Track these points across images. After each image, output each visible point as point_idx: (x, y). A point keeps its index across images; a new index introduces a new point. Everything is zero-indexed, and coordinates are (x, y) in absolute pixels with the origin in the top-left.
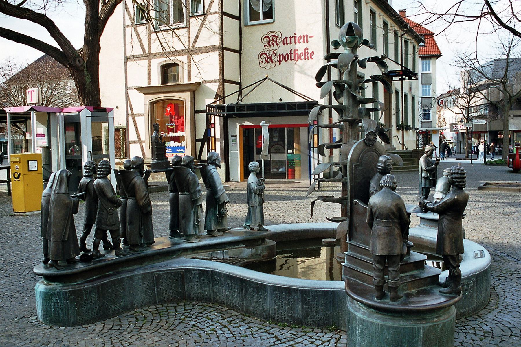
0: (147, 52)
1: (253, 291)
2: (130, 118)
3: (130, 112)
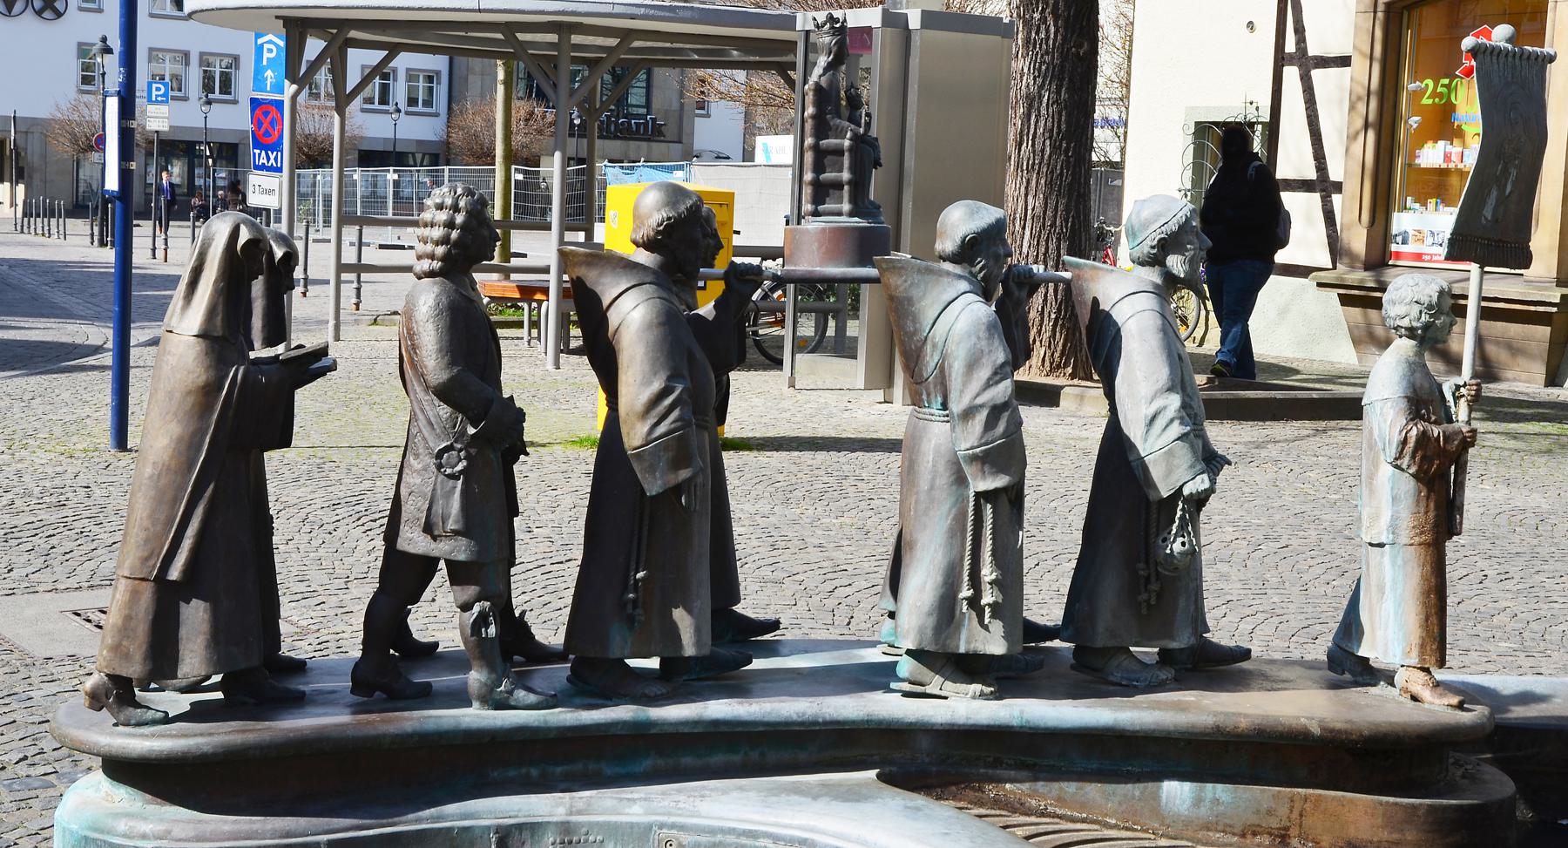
3: (1290, 47)
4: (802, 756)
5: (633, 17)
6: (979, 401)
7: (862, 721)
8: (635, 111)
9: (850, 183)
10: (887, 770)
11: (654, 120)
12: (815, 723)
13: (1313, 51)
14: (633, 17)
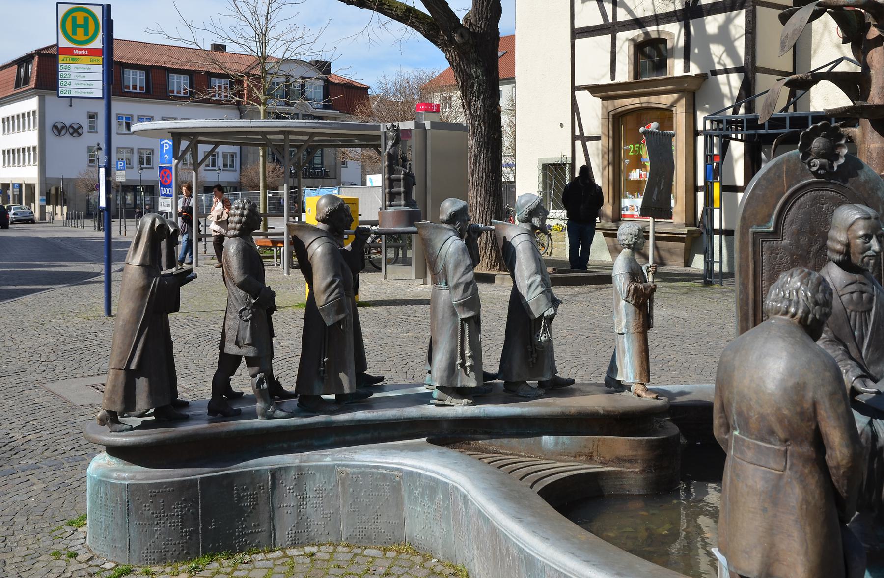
0: (611, 20)
1: (422, 497)
2: (578, 144)
3: (577, 133)
6: (460, 281)
12: (400, 419)
13: (586, 134)
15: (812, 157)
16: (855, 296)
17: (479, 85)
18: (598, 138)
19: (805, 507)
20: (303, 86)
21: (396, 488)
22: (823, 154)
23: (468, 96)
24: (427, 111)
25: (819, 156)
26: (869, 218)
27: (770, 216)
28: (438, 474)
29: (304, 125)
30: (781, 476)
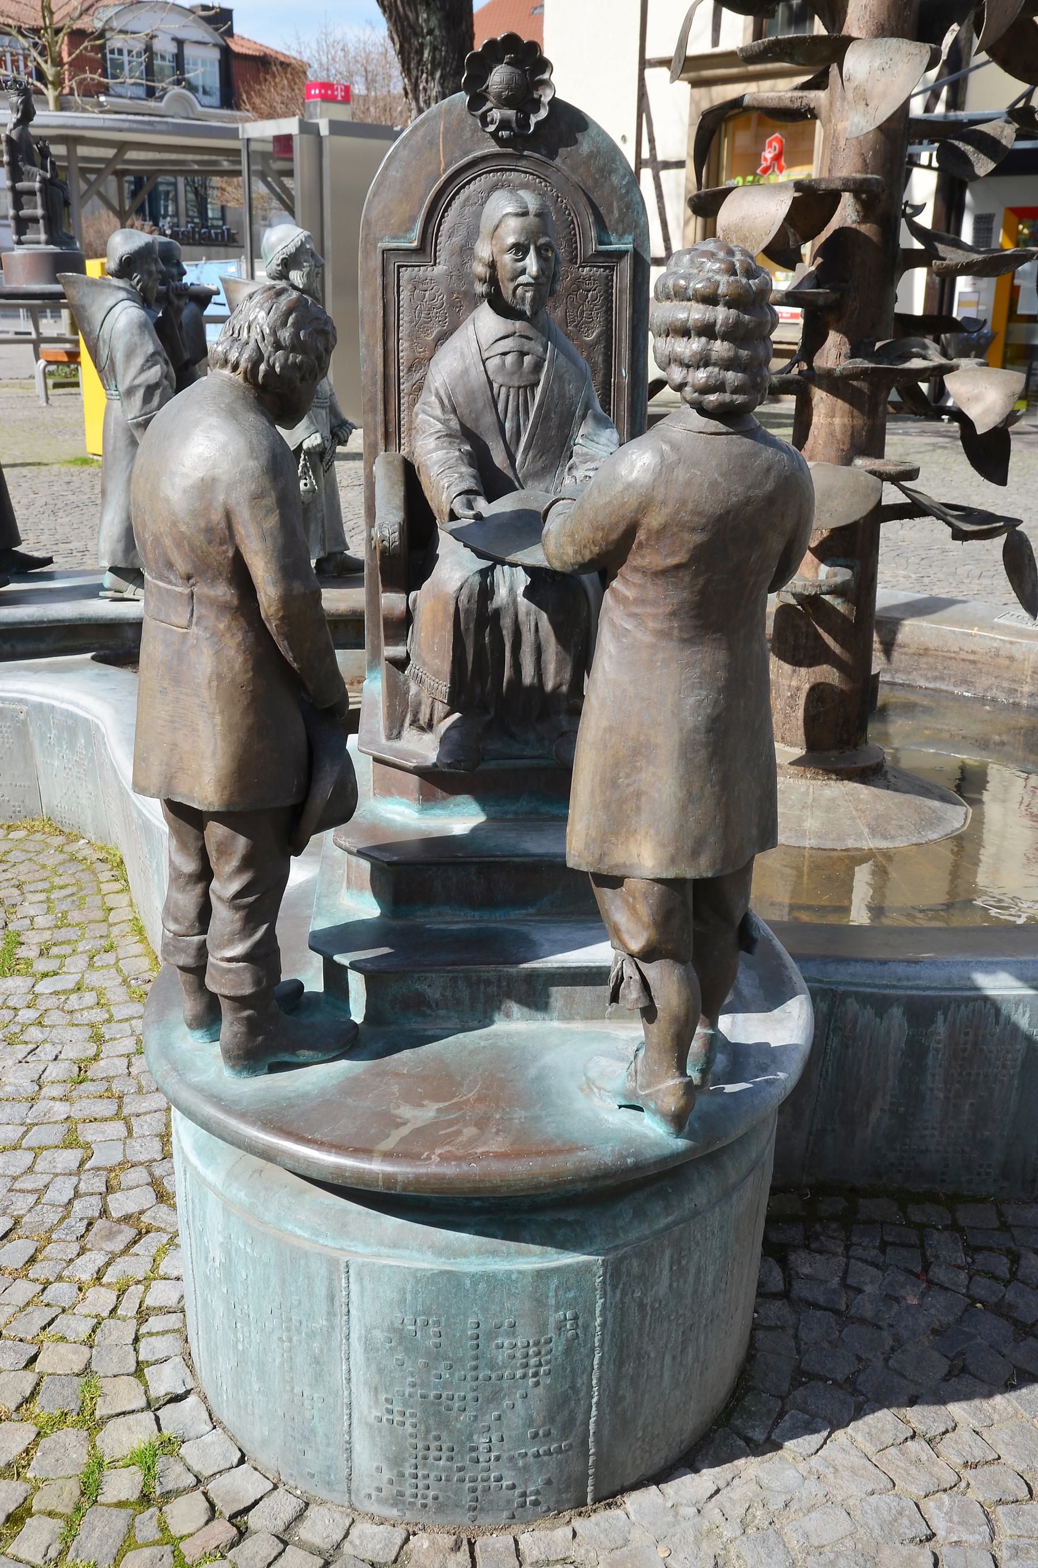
3: (645, 154)
4: (43, 647)
5: (120, 130)
6: (137, 382)
7: (76, 620)
8: (215, 223)
9: (43, 217)
10: (102, 653)
11: (228, 230)
12: (43, 622)
13: (660, 157)
14: (120, 130)
15: (489, 105)
16: (509, 359)
17: (434, 49)
18: (680, 164)
19: (214, 684)
20: (179, 59)
21: (21, 731)
22: (507, 98)
23: (414, 73)
24: (326, 98)
25: (504, 102)
26: (525, 214)
27: (413, 219)
28: (77, 705)
29: (100, 123)
30: (185, 635)
